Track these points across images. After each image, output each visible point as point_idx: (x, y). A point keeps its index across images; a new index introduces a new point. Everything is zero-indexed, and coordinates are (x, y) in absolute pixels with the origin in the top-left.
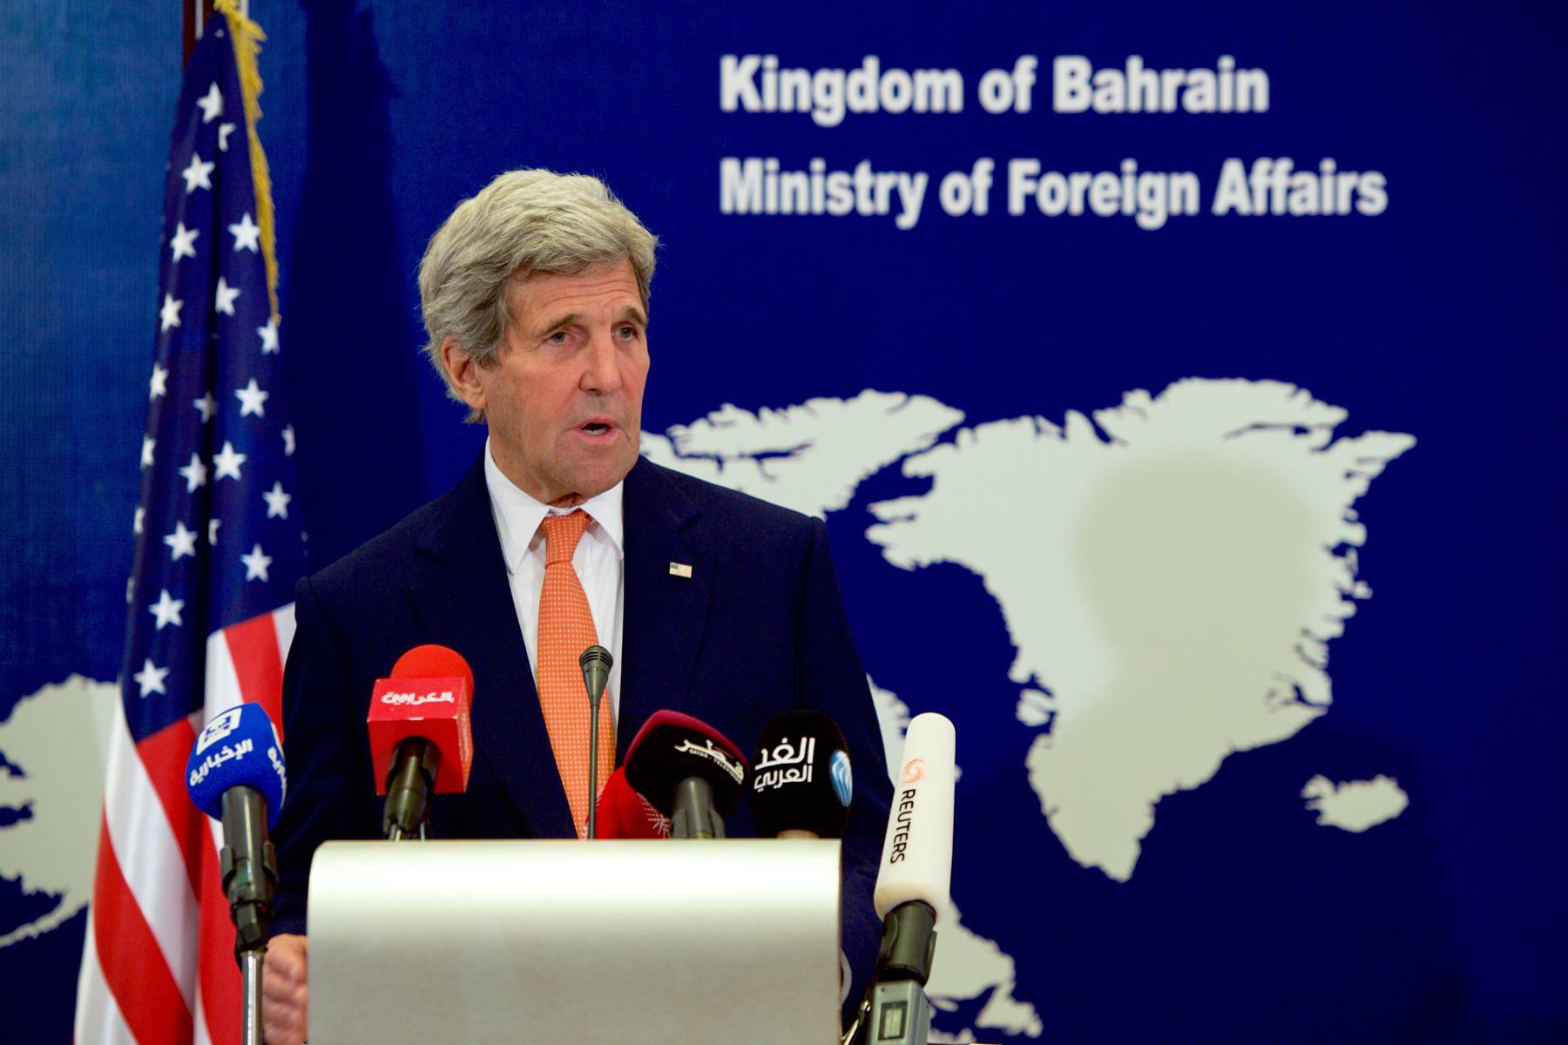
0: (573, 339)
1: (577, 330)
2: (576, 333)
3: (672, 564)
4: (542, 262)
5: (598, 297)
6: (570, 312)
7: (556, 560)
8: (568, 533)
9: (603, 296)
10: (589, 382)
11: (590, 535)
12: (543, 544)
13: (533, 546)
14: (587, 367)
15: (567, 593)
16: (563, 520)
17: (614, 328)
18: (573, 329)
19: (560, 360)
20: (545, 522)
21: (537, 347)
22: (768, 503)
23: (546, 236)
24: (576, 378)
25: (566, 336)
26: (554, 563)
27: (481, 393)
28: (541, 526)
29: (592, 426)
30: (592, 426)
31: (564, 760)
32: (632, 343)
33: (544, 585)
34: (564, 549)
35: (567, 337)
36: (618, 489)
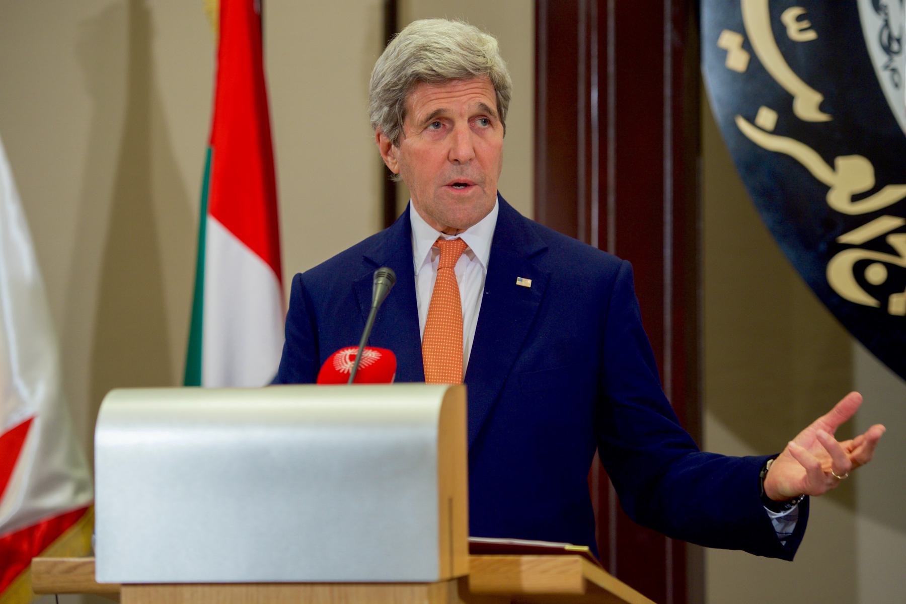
3: (519, 278)
5: (458, 98)
9: (462, 98)
10: (452, 156)
12: (437, 258)
17: (471, 120)
19: (436, 139)
21: (422, 132)
24: (444, 152)
27: (396, 163)
29: (457, 184)
30: (457, 184)
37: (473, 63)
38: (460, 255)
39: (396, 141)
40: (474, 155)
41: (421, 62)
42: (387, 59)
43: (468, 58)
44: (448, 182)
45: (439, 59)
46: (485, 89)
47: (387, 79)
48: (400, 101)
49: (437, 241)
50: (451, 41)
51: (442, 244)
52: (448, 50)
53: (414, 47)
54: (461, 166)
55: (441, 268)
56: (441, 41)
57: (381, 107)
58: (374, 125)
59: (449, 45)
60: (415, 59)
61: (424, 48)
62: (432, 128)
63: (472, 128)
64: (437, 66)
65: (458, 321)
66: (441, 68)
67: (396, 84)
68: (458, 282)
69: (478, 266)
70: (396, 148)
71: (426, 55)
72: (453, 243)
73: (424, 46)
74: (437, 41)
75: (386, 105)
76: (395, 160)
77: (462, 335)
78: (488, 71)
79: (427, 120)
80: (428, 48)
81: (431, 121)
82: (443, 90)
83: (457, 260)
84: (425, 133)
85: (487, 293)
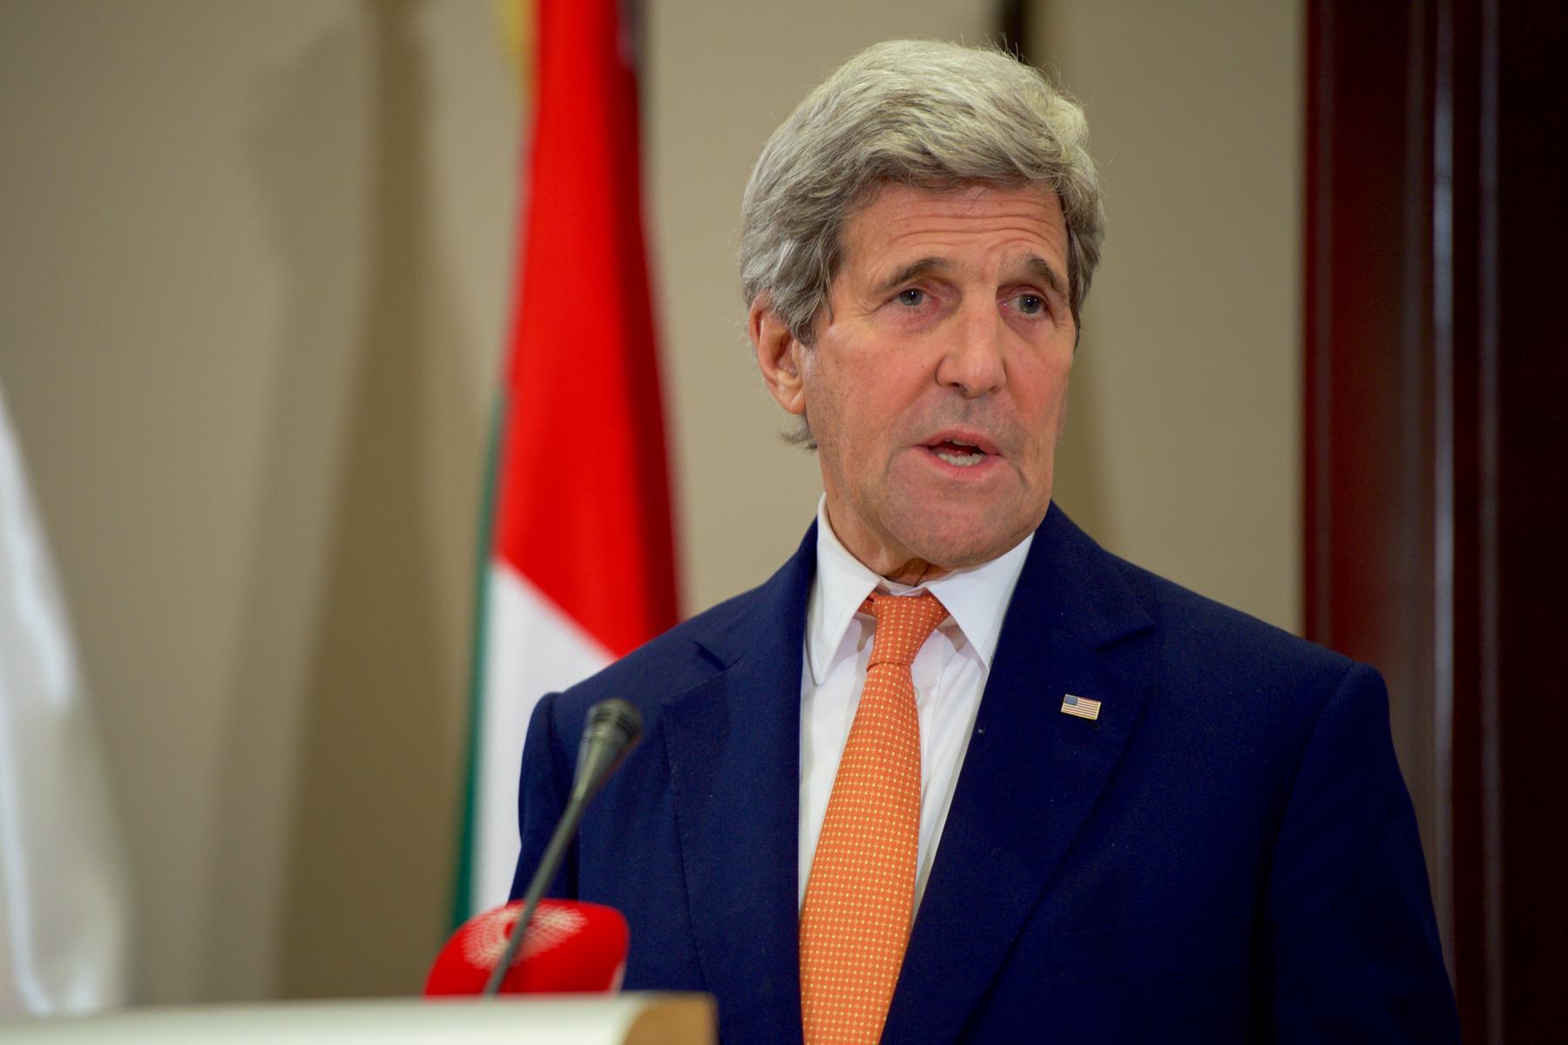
0: (935, 300)
1: (945, 289)
2: (944, 294)
3: (1099, 704)
5: (979, 236)
6: (930, 255)
9: (987, 235)
10: (948, 373)
11: (948, 641)
12: (870, 643)
14: (948, 348)
17: (1005, 290)
18: (936, 285)
21: (878, 309)
22: (1264, 623)
24: (929, 361)
25: (925, 296)
27: (799, 387)
31: (818, 1007)
32: (1038, 324)
33: (857, 719)
35: (925, 299)
37: (1027, 149)
38: (927, 634)
39: (806, 331)
40: (1003, 377)
41: (897, 131)
42: (801, 127)
43: (1015, 135)
44: (928, 435)
45: (943, 127)
46: (1047, 223)
47: (803, 171)
48: (830, 227)
49: (869, 599)
50: (975, 89)
51: (882, 607)
52: (968, 110)
53: (879, 97)
55: (875, 664)
56: (951, 87)
57: (777, 243)
58: (752, 286)
59: (969, 98)
60: (882, 122)
61: (908, 99)
63: (1004, 313)
64: (937, 142)
65: (908, 797)
66: (948, 148)
67: (823, 184)
68: (918, 703)
69: (973, 663)
70: (802, 347)
71: (909, 112)
72: (909, 604)
73: (907, 96)
74: (940, 87)
75: (792, 236)
76: (797, 379)
77: (917, 834)
78: (1060, 174)
79: (897, 281)
80: (916, 100)
82: (943, 208)
83: (924, 641)
85: (980, 731)
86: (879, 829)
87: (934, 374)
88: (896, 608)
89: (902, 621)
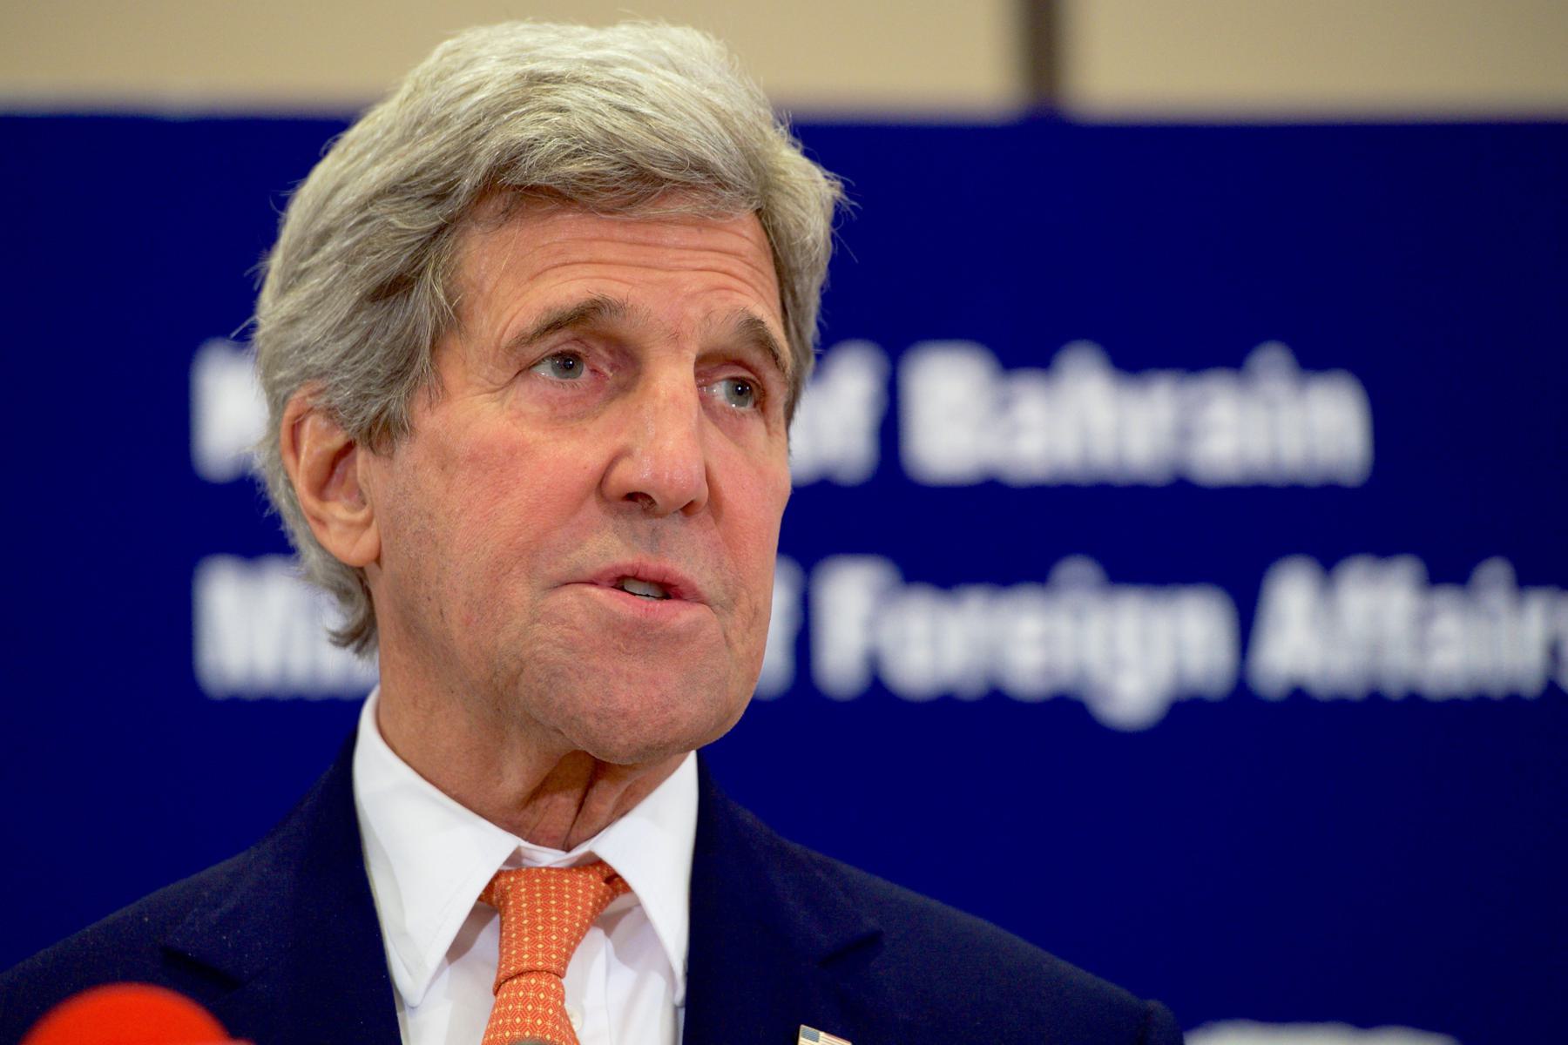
3: (803, 1027)
4: (543, 166)
5: (672, 275)
7: (525, 965)
8: (560, 907)
9: (685, 276)
13: (458, 950)
15: (549, 1024)
16: (549, 876)
17: (708, 364)
19: (561, 418)
20: (503, 880)
23: (560, 110)
26: (520, 974)
27: (367, 524)
28: (490, 888)
34: (547, 942)
36: (690, 765)
40: (705, 490)
54: (655, 521)
62: (545, 371)
81: (556, 341)
84: (522, 389)
86: (529, 1021)
87: (600, 484)
88: (526, 885)
89: (538, 888)
